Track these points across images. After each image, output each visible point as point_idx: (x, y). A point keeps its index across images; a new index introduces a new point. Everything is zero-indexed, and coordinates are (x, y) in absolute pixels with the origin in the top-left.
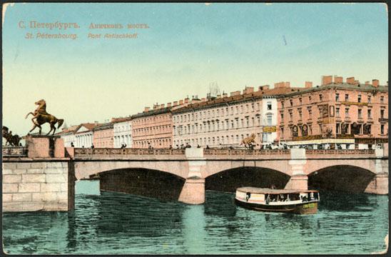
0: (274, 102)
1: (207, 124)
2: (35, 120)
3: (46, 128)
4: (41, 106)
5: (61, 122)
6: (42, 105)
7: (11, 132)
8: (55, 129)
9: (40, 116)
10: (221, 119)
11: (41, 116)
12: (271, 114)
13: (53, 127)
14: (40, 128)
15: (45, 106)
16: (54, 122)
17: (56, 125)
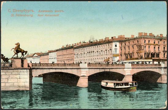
0: (118, 44)
1: (89, 53)
2: (15, 51)
3: (20, 55)
4: (18, 45)
5: (26, 52)
6: (18, 45)
7: (5, 57)
8: (24, 55)
9: (17, 50)
10: (95, 51)
11: (18, 50)
12: (116, 49)
13: (23, 54)
14: (17, 55)
15: (19, 45)
16: (23, 52)
17: (24, 54)
